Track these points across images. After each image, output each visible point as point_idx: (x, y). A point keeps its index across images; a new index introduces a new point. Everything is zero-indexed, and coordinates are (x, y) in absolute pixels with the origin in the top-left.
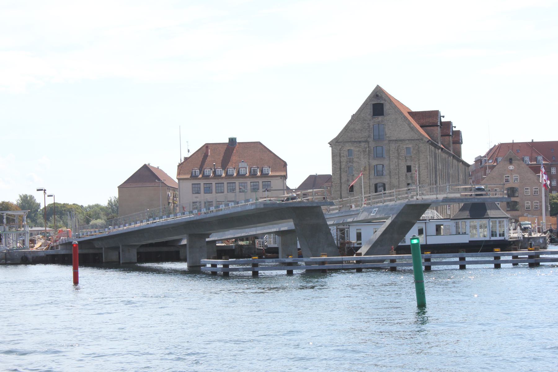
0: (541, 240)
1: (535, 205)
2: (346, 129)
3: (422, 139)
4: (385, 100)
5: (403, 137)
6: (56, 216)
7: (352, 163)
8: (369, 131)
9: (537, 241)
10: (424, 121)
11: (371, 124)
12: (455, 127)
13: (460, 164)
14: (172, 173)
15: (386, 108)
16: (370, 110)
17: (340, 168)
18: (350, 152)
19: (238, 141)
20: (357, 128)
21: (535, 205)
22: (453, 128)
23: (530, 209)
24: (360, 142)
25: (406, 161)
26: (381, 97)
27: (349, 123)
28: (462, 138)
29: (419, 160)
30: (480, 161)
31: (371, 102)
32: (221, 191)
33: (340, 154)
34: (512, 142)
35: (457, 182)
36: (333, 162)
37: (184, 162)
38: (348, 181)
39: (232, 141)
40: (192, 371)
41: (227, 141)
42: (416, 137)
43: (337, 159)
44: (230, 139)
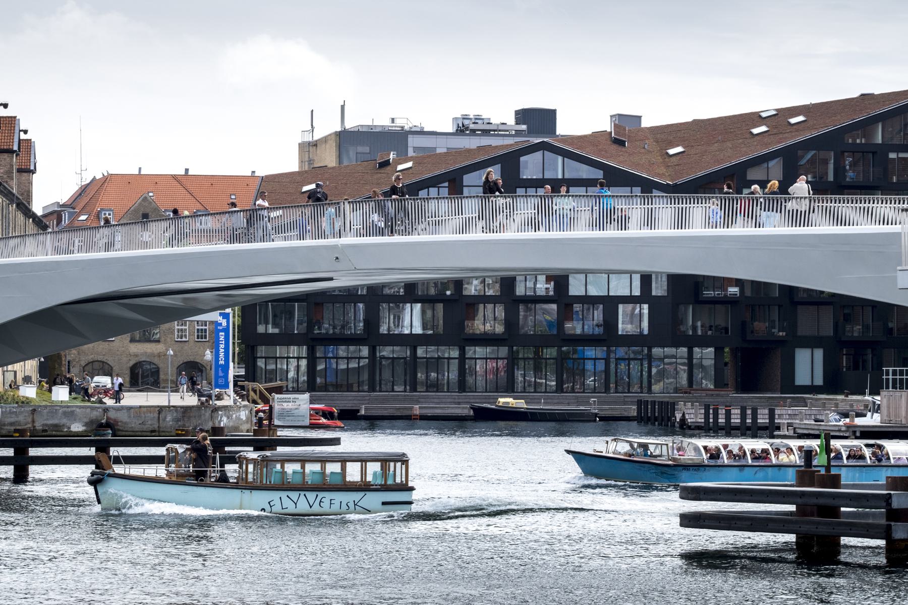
0: (244, 412)
1: (198, 330)
6: (367, 360)
9: (234, 416)
12: (26, 132)
13: (29, 221)
21: (198, 330)
22: (22, 133)
23: (206, 338)
30: (55, 215)
32: (629, 365)
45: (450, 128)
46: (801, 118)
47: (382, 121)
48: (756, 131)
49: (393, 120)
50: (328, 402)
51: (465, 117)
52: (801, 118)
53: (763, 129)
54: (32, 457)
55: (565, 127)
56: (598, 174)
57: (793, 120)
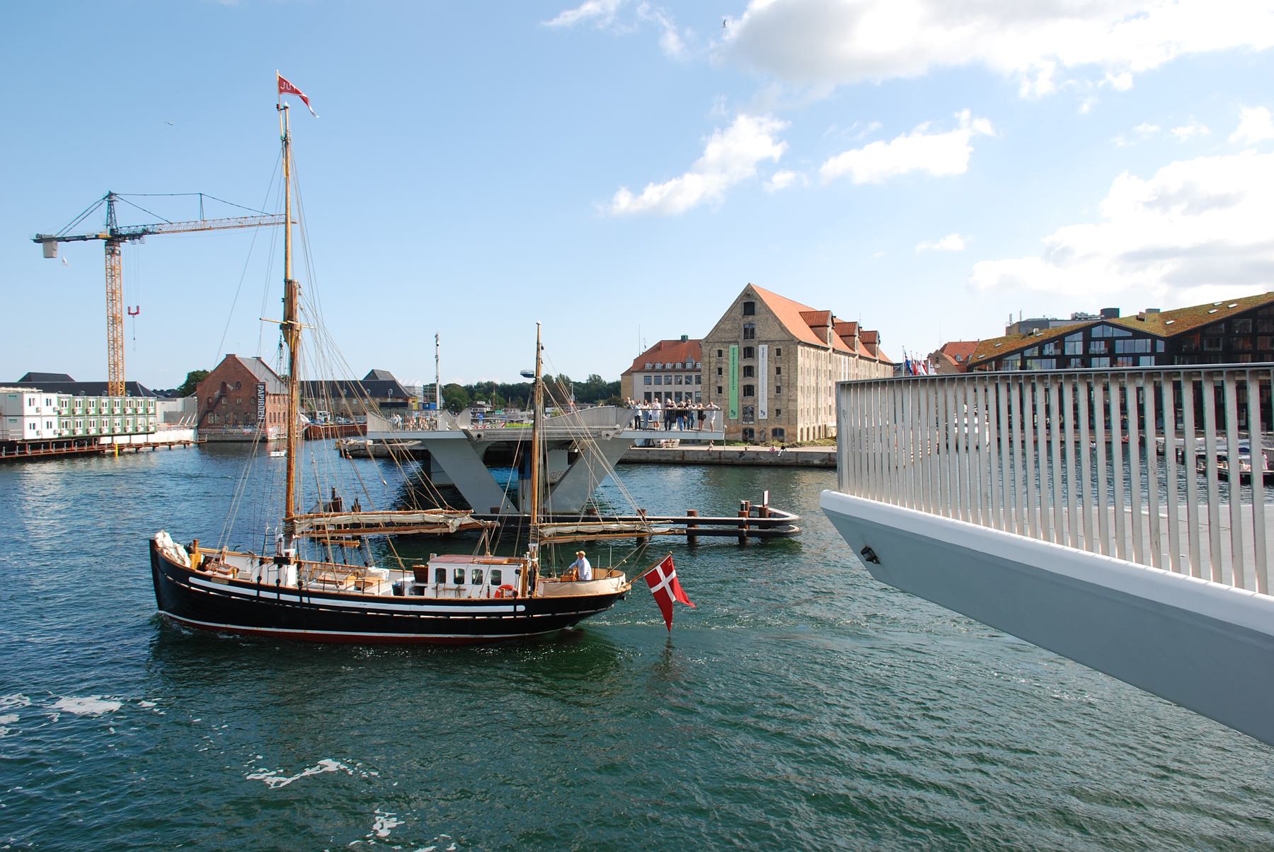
3: (792, 340)
5: (773, 338)
16: (741, 309)
18: (720, 353)
38: (717, 382)
42: (787, 337)
47: (1038, 316)
55: (1161, 311)
56: (1130, 334)
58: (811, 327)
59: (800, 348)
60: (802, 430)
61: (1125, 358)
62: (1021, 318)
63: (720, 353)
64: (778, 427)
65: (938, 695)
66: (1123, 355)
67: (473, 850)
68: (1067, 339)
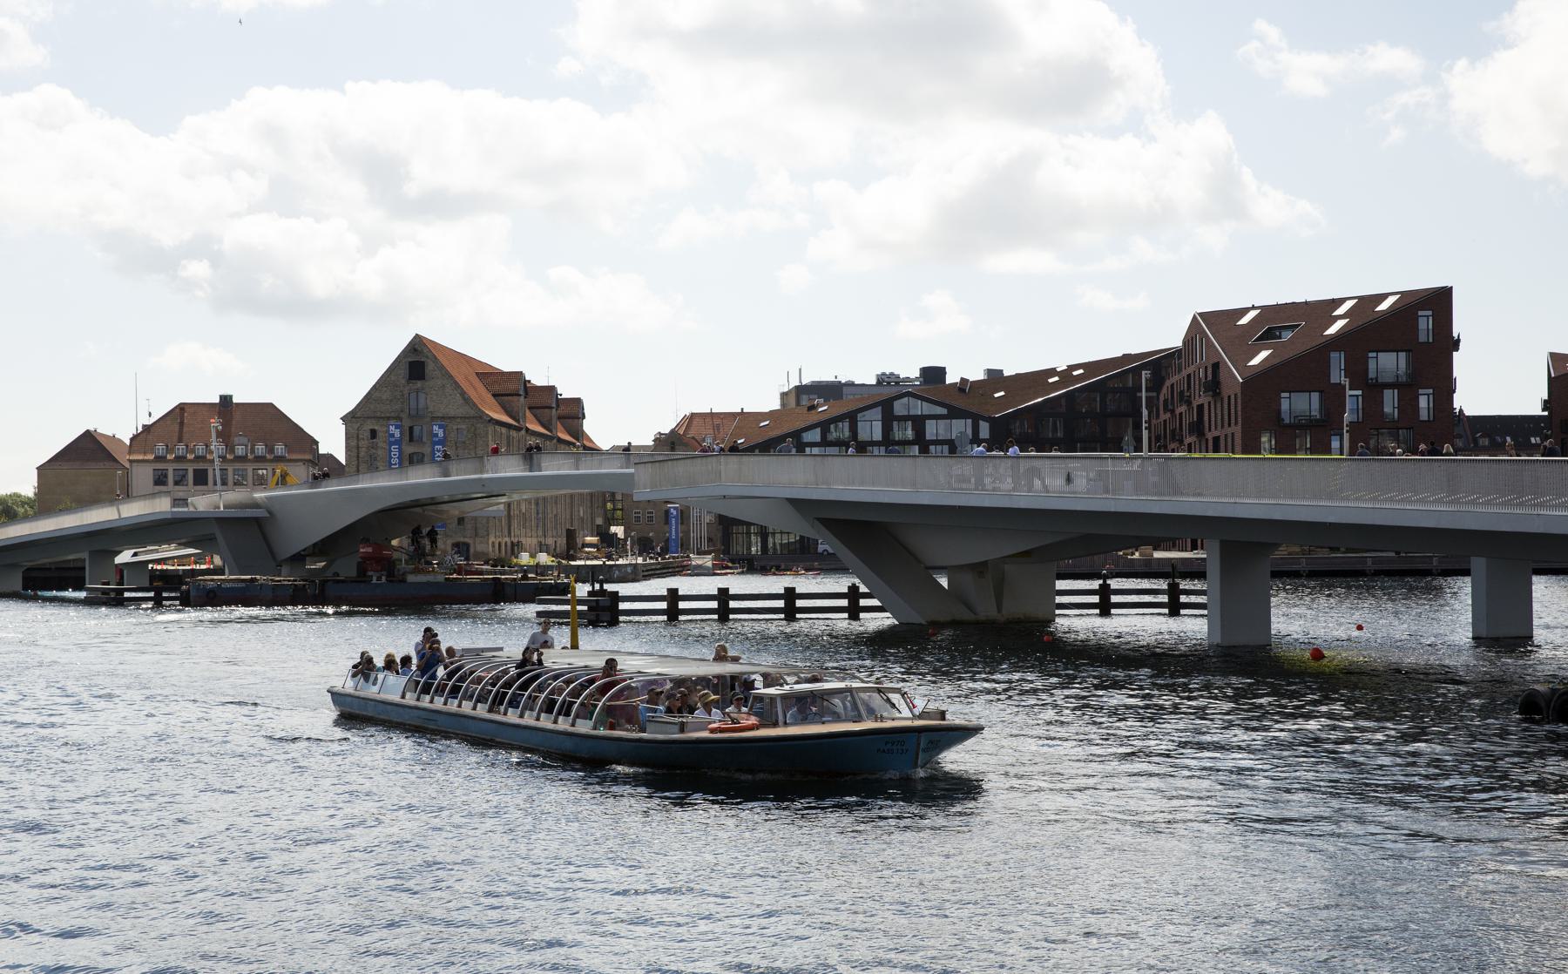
2: (368, 398)
3: (481, 417)
4: (427, 357)
5: (452, 413)
7: (376, 449)
8: (402, 403)
10: (497, 389)
11: (406, 392)
12: (561, 395)
14: (333, 442)
15: (430, 367)
16: (404, 371)
17: (358, 457)
18: (373, 434)
19: (235, 400)
20: (384, 397)
24: (389, 418)
25: (456, 449)
26: (422, 352)
27: (372, 389)
28: (583, 409)
29: (476, 447)
31: (406, 360)
33: (358, 436)
34: (709, 411)
35: (1219, 427)
36: (346, 447)
37: (141, 432)
39: (226, 400)
40: (784, 967)
41: (217, 400)
42: (472, 413)
43: (354, 443)
44: (221, 397)
45: (874, 382)
46: (1081, 371)
47: (827, 376)
48: (1051, 380)
49: (836, 377)
50: (179, 541)
51: (884, 374)
52: (1081, 371)
53: (1056, 379)
54: (845, 598)
55: (952, 378)
56: (944, 411)
57: (1075, 373)
58: (494, 395)
59: (491, 428)
60: (1236, 423)
61: (939, 448)
62: (801, 382)
63: (373, 434)
64: (462, 540)
65: (1192, 935)
66: (937, 442)
67: (1393, 970)
68: (859, 415)
